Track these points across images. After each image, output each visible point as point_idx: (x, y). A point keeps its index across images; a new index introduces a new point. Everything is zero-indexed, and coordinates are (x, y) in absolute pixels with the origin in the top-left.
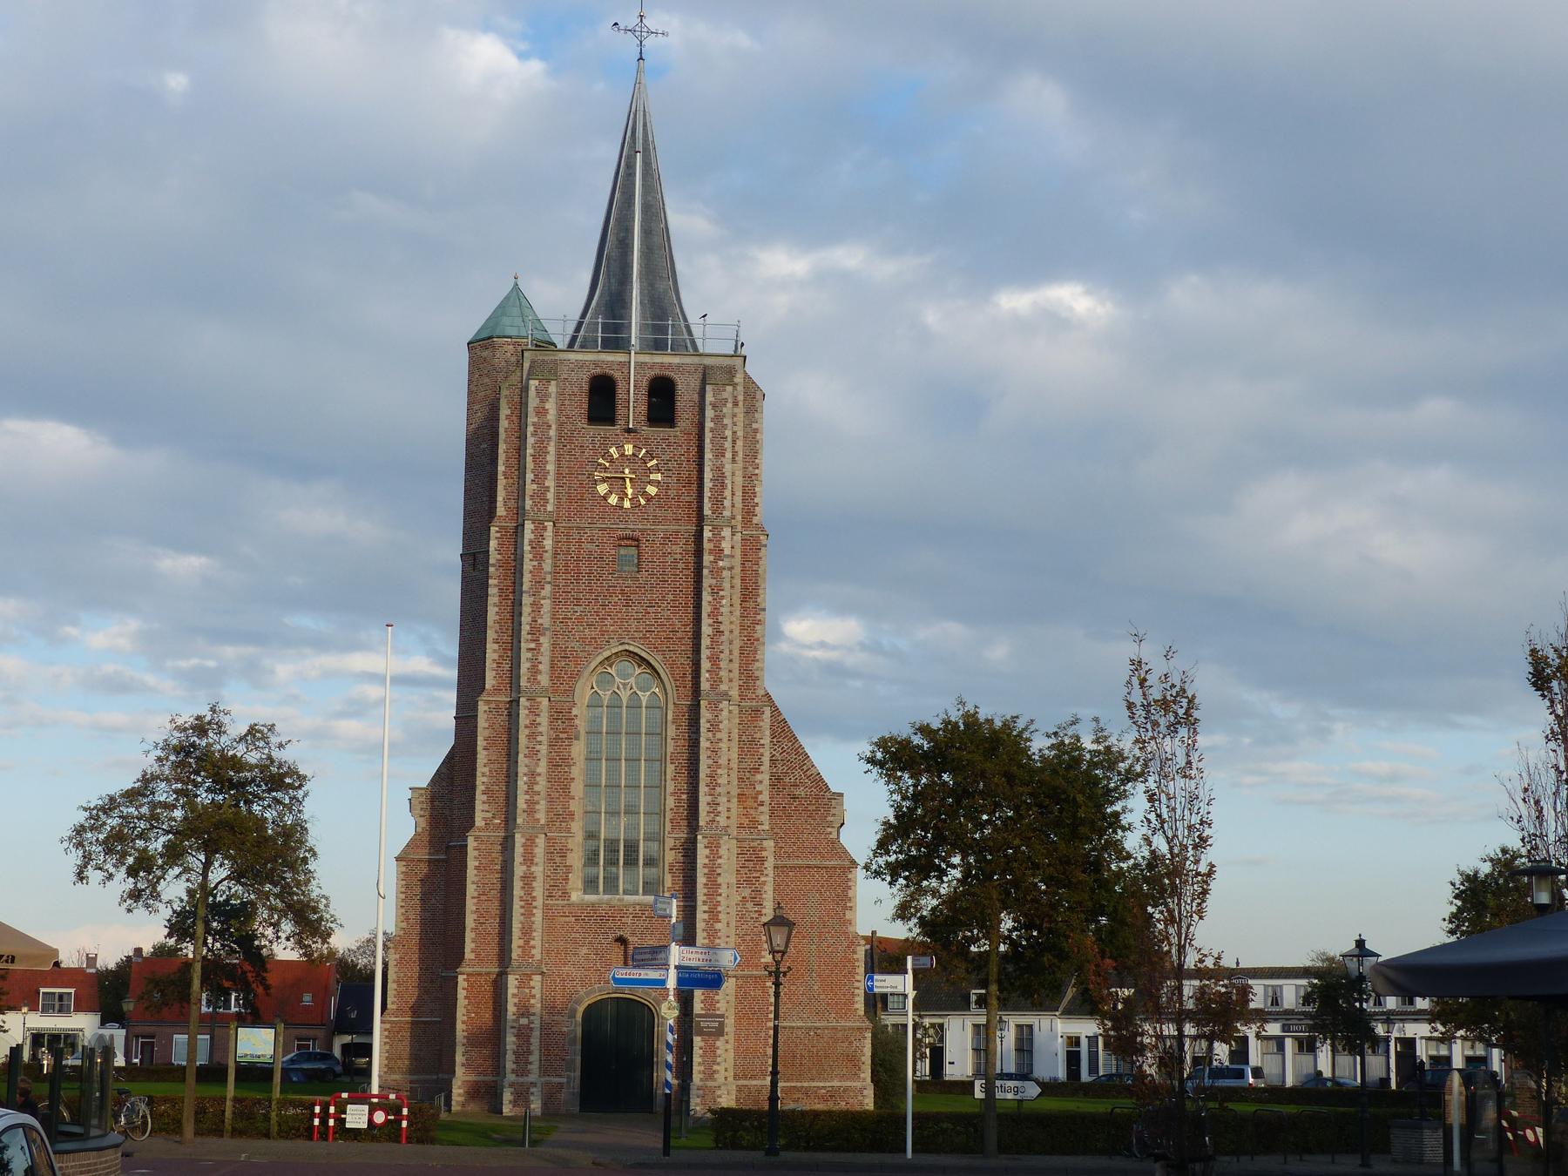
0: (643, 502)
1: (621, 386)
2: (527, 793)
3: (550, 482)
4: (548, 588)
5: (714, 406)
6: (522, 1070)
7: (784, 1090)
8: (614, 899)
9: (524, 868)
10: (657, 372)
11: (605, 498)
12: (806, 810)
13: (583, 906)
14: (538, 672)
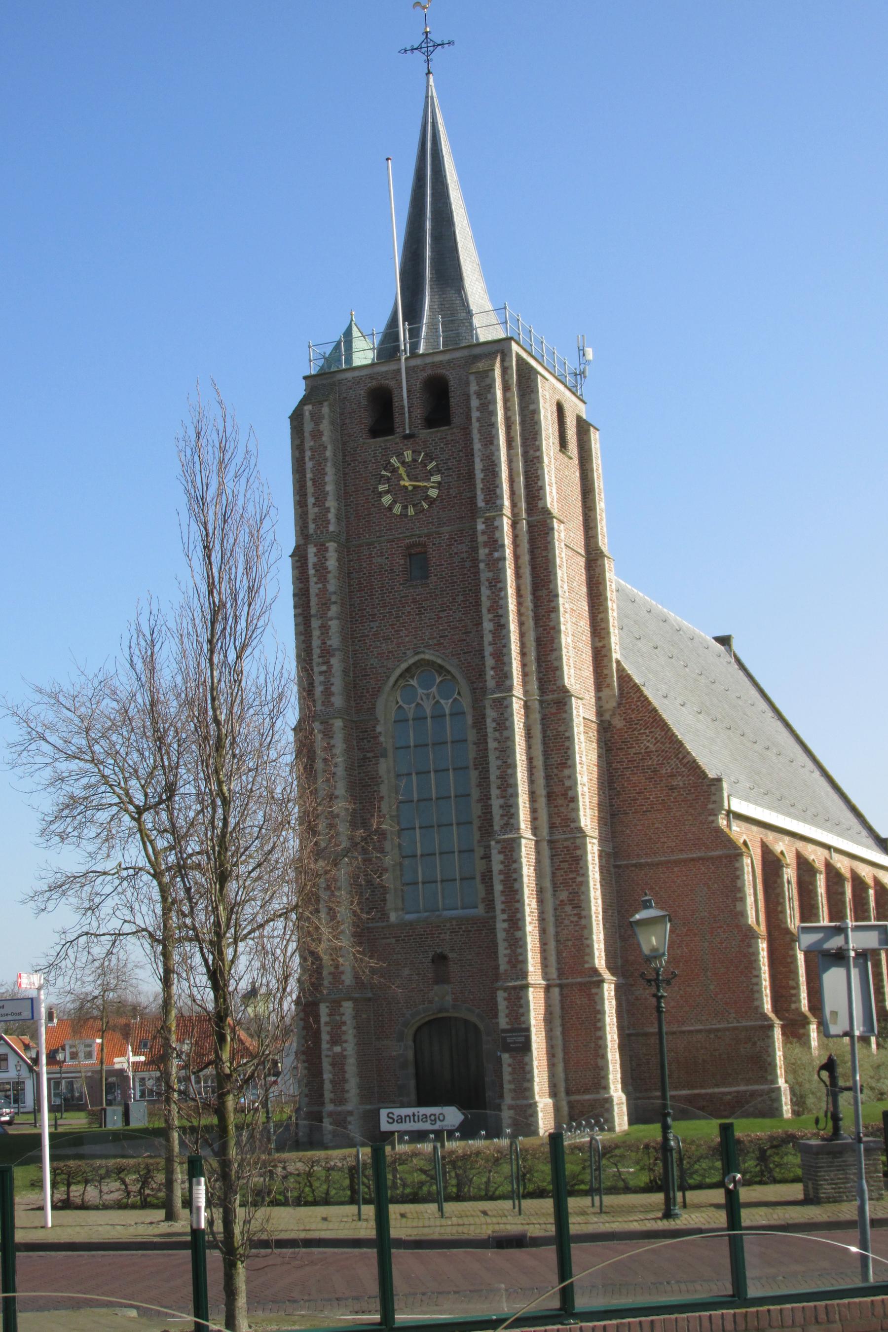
0: (426, 506)
1: (395, 393)
3: (331, 503)
5: (479, 395)
6: (340, 1100)
11: (390, 508)
14: (332, 694)
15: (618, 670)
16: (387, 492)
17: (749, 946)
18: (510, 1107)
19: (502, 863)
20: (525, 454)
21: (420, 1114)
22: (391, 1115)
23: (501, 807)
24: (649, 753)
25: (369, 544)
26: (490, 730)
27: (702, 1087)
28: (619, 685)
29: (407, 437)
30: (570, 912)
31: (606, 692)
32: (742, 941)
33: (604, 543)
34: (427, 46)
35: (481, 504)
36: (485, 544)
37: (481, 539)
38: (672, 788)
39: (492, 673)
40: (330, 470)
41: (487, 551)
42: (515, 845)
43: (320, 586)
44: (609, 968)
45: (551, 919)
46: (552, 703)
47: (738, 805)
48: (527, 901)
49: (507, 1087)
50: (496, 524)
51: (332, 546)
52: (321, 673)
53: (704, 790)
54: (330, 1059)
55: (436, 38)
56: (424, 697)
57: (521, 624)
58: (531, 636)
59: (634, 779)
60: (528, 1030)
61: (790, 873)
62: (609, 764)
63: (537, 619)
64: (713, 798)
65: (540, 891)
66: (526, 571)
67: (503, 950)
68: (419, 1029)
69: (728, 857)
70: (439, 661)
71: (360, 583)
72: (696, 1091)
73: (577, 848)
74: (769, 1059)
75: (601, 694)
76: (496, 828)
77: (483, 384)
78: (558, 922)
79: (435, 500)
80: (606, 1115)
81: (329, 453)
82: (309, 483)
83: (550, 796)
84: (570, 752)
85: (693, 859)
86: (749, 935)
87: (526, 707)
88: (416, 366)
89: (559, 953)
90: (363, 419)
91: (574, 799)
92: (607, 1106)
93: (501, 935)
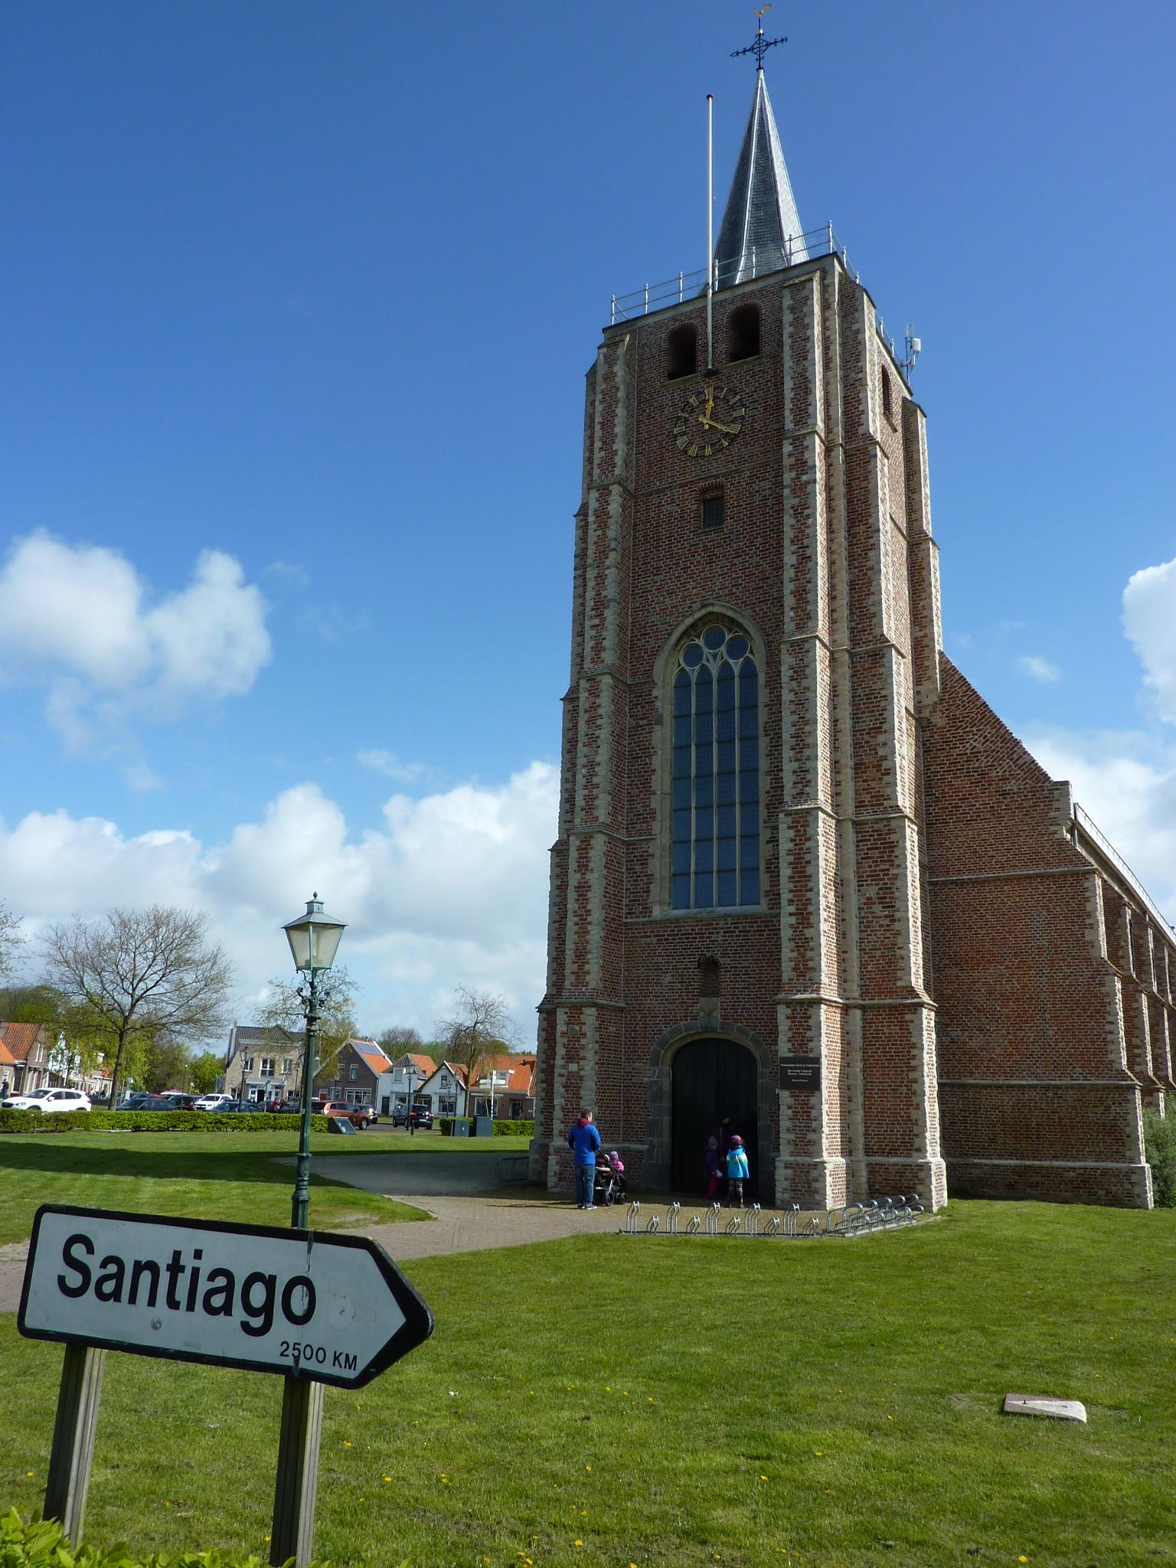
2: (585, 787)
3: (620, 446)
4: (612, 555)
5: (792, 309)
7: (16, 1239)
8: (703, 913)
9: (578, 876)
12: (1020, 807)
13: (666, 922)
15: (940, 663)
16: (684, 434)
17: (1102, 984)
18: (787, 1166)
19: (792, 840)
20: (845, 378)
21: (206, 1267)
22: (78, 1251)
23: (795, 772)
24: (976, 754)
25: (658, 492)
26: (785, 679)
27: (1035, 1158)
28: (942, 679)
29: (710, 374)
30: (879, 914)
31: (926, 686)
32: (1093, 977)
33: (928, 526)
34: (760, 47)
35: (789, 425)
36: (792, 467)
37: (787, 462)
38: (1004, 794)
39: (792, 614)
40: (620, 411)
41: (793, 474)
42: (810, 818)
43: (599, 532)
44: (927, 988)
48: (822, 891)
49: (785, 1136)
50: (806, 443)
51: (616, 489)
52: (593, 627)
54: (564, 1080)
56: (711, 658)
57: (831, 563)
58: (843, 577)
62: (927, 766)
63: (851, 558)
64: (1056, 805)
65: (839, 883)
66: (841, 504)
67: (787, 952)
70: (730, 613)
71: (646, 535)
72: (1027, 1163)
73: (891, 831)
74: (1128, 1130)
75: (919, 688)
76: (787, 798)
77: (799, 297)
78: (865, 925)
79: (736, 436)
80: (919, 1188)
81: (621, 394)
82: (598, 427)
84: (886, 714)
85: (1029, 877)
87: (833, 660)
88: (725, 300)
89: (863, 966)
91: (890, 772)
92: (921, 1175)
93: (786, 933)
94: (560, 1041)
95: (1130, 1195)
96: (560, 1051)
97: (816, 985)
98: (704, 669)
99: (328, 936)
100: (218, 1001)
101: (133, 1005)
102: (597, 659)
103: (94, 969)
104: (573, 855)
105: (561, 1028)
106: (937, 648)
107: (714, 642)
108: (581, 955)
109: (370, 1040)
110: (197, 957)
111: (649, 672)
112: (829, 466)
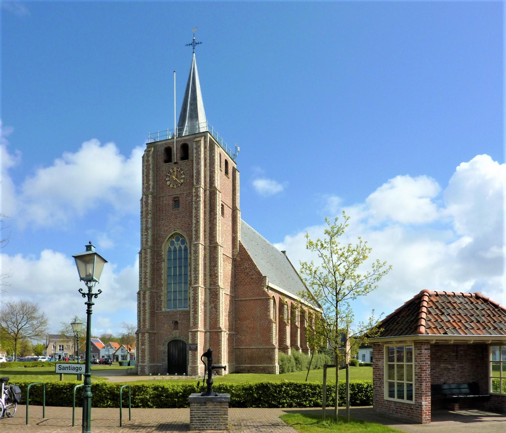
3: (151, 183)
4: (150, 215)
5: (196, 149)
8: (174, 310)
10: (183, 142)
13: (166, 312)
20: (210, 170)
29: (176, 163)
31: (235, 250)
33: (238, 206)
34: (194, 44)
35: (195, 184)
37: (194, 194)
40: (151, 172)
45: (208, 312)
46: (213, 248)
47: (270, 285)
48: (200, 306)
51: (150, 196)
53: (261, 279)
55: (197, 41)
59: (242, 275)
60: (197, 344)
61: (297, 313)
62: (235, 271)
63: (210, 221)
65: (205, 304)
66: (208, 206)
67: (192, 320)
68: (170, 343)
69: (266, 299)
73: (217, 291)
76: (192, 283)
78: (211, 313)
81: (151, 167)
83: (211, 275)
86: (270, 322)
87: (205, 248)
89: (210, 322)
90: (162, 157)
93: (191, 316)
94: (140, 341)
95: (273, 371)
96: (140, 343)
97: (197, 327)
98: (175, 247)
99: (79, 325)
100: (45, 329)
101: (18, 331)
102: (147, 244)
103: (4, 320)
104: (142, 296)
105: (140, 338)
106: (238, 239)
107: (178, 240)
108: (144, 321)
109: (97, 338)
110: (37, 316)
111: (161, 247)
112: (205, 195)
